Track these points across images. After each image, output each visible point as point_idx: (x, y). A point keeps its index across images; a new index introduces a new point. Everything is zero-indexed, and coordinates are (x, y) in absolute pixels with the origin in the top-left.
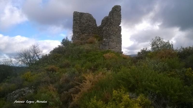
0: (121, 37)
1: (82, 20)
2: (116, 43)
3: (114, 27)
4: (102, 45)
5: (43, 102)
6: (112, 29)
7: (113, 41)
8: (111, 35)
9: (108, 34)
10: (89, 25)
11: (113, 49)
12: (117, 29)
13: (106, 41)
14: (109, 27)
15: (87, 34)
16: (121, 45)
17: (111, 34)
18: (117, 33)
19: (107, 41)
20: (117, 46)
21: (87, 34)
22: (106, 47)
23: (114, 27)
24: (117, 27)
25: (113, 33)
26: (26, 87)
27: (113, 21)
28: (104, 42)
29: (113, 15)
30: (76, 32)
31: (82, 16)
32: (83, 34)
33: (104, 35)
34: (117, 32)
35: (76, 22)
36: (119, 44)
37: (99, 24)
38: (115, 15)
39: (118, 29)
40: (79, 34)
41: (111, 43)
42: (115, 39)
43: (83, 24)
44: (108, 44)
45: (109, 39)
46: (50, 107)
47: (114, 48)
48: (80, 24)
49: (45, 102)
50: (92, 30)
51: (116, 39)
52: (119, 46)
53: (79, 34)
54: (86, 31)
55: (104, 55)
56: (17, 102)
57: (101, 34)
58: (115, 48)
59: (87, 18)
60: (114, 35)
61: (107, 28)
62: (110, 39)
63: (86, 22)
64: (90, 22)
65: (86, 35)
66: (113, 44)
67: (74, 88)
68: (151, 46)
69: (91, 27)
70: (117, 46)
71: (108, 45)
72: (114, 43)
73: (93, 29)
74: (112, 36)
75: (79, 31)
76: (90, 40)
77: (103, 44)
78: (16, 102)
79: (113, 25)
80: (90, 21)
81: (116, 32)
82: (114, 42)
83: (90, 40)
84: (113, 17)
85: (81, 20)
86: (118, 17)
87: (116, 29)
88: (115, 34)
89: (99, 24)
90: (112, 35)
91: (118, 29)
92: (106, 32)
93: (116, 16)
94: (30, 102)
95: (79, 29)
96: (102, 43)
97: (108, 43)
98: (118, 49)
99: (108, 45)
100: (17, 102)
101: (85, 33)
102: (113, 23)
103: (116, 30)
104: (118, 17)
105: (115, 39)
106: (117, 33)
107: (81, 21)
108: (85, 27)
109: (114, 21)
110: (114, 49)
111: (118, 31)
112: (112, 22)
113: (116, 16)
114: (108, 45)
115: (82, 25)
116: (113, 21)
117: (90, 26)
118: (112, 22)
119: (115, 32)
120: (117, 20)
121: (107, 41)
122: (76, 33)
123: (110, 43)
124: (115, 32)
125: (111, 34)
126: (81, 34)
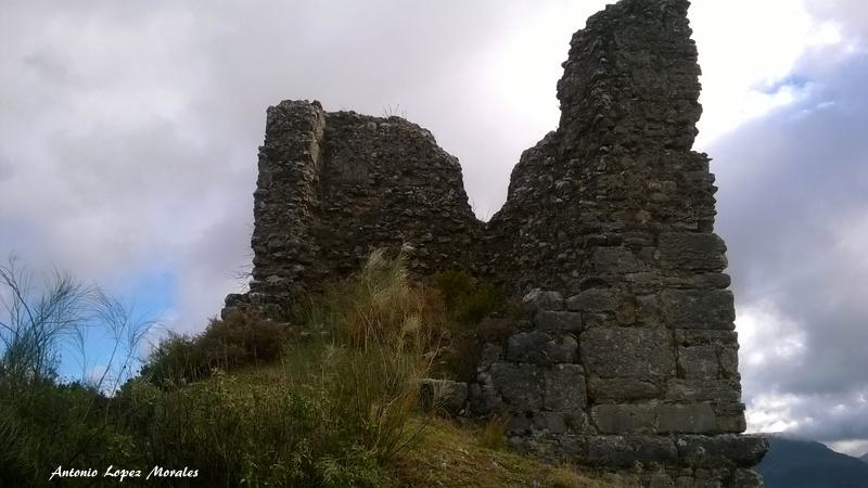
0: (723, 265)
1: (346, 167)
2: (663, 333)
3: (625, 161)
4: (505, 357)
6: (614, 181)
7: (629, 310)
8: (605, 243)
9: (571, 237)
10: (404, 201)
11: (632, 400)
12: (660, 177)
13: (550, 304)
14: (576, 167)
16: (734, 360)
17: (597, 230)
18: (665, 219)
19: (565, 306)
20: (681, 373)
22: (546, 374)
23: (625, 161)
24: (661, 163)
25: (620, 223)
26: (649, 399)
27: (615, 108)
28: (529, 328)
29: (605, 47)
30: (278, 255)
31: (342, 137)
33: (521, 261)
35: (279, 169)
36: (709, 348)
37: (487, 197)
38: (632, 49)
39: (678, 176)
40: (299, 267)
42: (655, 288)
44: (571, 341)
45: (586, 285)
46: (511, 486)
49: (189, 475)
50: (430, 236)
51: (667, 285)
52: (704, 365)
53: (299, 267)
55: (638, 298)
56: (66, 473)
57: (501, 275)
58: (660, 395)
60: (636, 248)
61: (558, 177)
63: (378, 183)
66: (636, 347)
69: (422, 218)
70: (681, 373)
71: (578, 357)
73: (437, 233)
74: (621, 257)
75: (303, 249)
77: (515, 341)
78: (59, 472)
79: (618, 147)
80: (407, 173)
81: (655, 215)
82: (638, 324)
84: (611, 63)
85: (336, 161)
87: (652, 185)
89: (487, 197)
90: (616, 242)
92: (548, 223)
93: (645, 58)
94: (123, 476)
95: (303, 228)
96: (501, 338)
97: (577, 333)
99: (578, 350)
100: (66, 473)
102: (617, 120)
103: (657, 196)
105: (655, 288)
107: (336, 173)
109: (626, 106)
110: (654, 403)
111: (679, 206)
112: (600, 109)
114: (578, 357)
115: (339, 198)
116: (615, 99)
117: (408, 211)
118: (600, 109)
121: (565, 306)
122: (278, 260)
124: (644, 216)
125: (597, 230)
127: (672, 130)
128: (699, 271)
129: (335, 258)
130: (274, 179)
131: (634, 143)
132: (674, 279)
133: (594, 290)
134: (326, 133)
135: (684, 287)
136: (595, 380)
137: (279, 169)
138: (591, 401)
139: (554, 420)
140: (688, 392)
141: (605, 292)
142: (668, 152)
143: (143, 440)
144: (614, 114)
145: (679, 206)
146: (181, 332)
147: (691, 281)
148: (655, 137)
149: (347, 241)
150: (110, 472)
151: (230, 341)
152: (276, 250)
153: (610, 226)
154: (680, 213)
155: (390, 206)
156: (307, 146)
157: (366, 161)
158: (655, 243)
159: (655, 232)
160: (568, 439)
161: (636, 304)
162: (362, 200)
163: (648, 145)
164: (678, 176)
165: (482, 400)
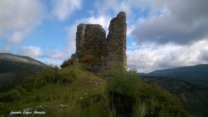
3: (113, 41)
5: (41, 113)
6: (111, 43)
15: (92, 50)
17: (108, 50)
21: (92, 50)
23: (113, 41)
24: (117, 41)
25: (111, 49)
32: (88, 49)
34: (117, 47)
35: (79, 36)
38: (115, 25)
39: (119, 43)
40: (81, 49)
41: (108, 62)
43: (89, 37)
44: (104, 63)
48: (86, 38)
49: (43, 113)
53: (81, 49)
54: (91, 46)
56: (14, 113)
59: (95, 30)
60: (113, 52)
63: (93, 36)
64: (97, 35)
65: (91, 50)
71: (105, 65)
74: (111, 53)
75: (82, 47)
76: (85, 58)
78: (13, 113)
79: (112, 39)
83: (85, 58)
84: (112, 27)
85: (87, 33)
86: (119, 27)
88: (115, 50)
90: (110, 51)
91: (119, 44)
94: (27, 113)
100: (14, 113)
101: (90, 48)
102: (112, 35)
103: (116, 45)
104: (119, 27)
107: (87, 35)
108: (91, 41)
111: (119, 46)
113: (117, 26)
119: (114, 48)
120: (118, 31)
123: (107, 62)
124: (114, 48)
125: (108, 50)
126: (85, 50)
127: (119, 36)
129: (86, 48)
130: (78, 37)
131: (114, 38)
133: (107, 57)
134: (86, 29)
135: (118, 56)
136: (106, 67)
137: (79, 36)
138: (106, 69)
139: (101, 71)
141: (108, 57)
142: (118, 39)
143: (41, 101)
144: (112, 34)
145: (119, 46)
146: (66, 60)
147: (119, 56)
148: (117, 37)
149: (88, 45)
151: (69, 62)
152: (78, 47)
153: (110, 49)
154: (119, 47)
155: (95, 39)
157: (91, 32)
158: (115, 51)
159: (115, 50)
160: (103, 73)
161: (112, 58)
162: (91, 38)
163: (116, 38)
164: (119, 43)
165: (94, 69)
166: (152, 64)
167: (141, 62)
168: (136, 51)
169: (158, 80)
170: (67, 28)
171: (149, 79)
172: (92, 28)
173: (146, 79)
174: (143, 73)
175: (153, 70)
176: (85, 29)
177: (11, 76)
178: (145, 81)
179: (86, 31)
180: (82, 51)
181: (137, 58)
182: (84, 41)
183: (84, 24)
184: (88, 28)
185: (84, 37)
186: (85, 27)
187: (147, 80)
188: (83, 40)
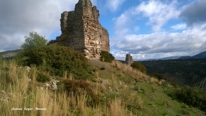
18: (80, 27)
24: (79, 22)
32: (70, 32)
38: (77, 9)
40: (65, 32)
44: (72, 40)
47: (78, 43)
49: (44, 109)
52: (82, 41)
53: (65, 32)
56: (15, 109)
60: (77, 30)
62: (74, 34)
67: (191, 109)
68: (28, 36)
71: (72, 41)
72: (77, 38)
74: (75, 32)
75: (65, 30)
87: (79, 24)
90: (75, 30)
91: (81, 24)
94: (28, 110)
98: (81, 44)
100: (15, 109)
101: (71, 30)
103: (79, 25)
106: (80, 27)
114: (72, 41)
126: (68, 33)
128: (82, 32)
132: (80, 33)
134: (68, 15)
140: (80, 43)
145: (81, 26)
147: (81, 33)
150: (26, 109)
156: (20, 110)
161: (77, 36)
166: (198, 45)
167: (188, 44)
168: (184, 32)
169: (203, 62)
170: (114, 19)
171: (193, 62)
172: (72, 14)
173: (190, 62)
174: (188, 56)
175: (201, 52)
176: (67, 15)
177: (174, 80)
178: (189, 64)
179: (69, 17)
180: (65, 33)
181: (184, 39)
182: (67, 25)
183: (66, 12)
184: (70, 14)
185: (66, 22)
186: (68, 14)
187: (191, 63)
188: (66, 25)
